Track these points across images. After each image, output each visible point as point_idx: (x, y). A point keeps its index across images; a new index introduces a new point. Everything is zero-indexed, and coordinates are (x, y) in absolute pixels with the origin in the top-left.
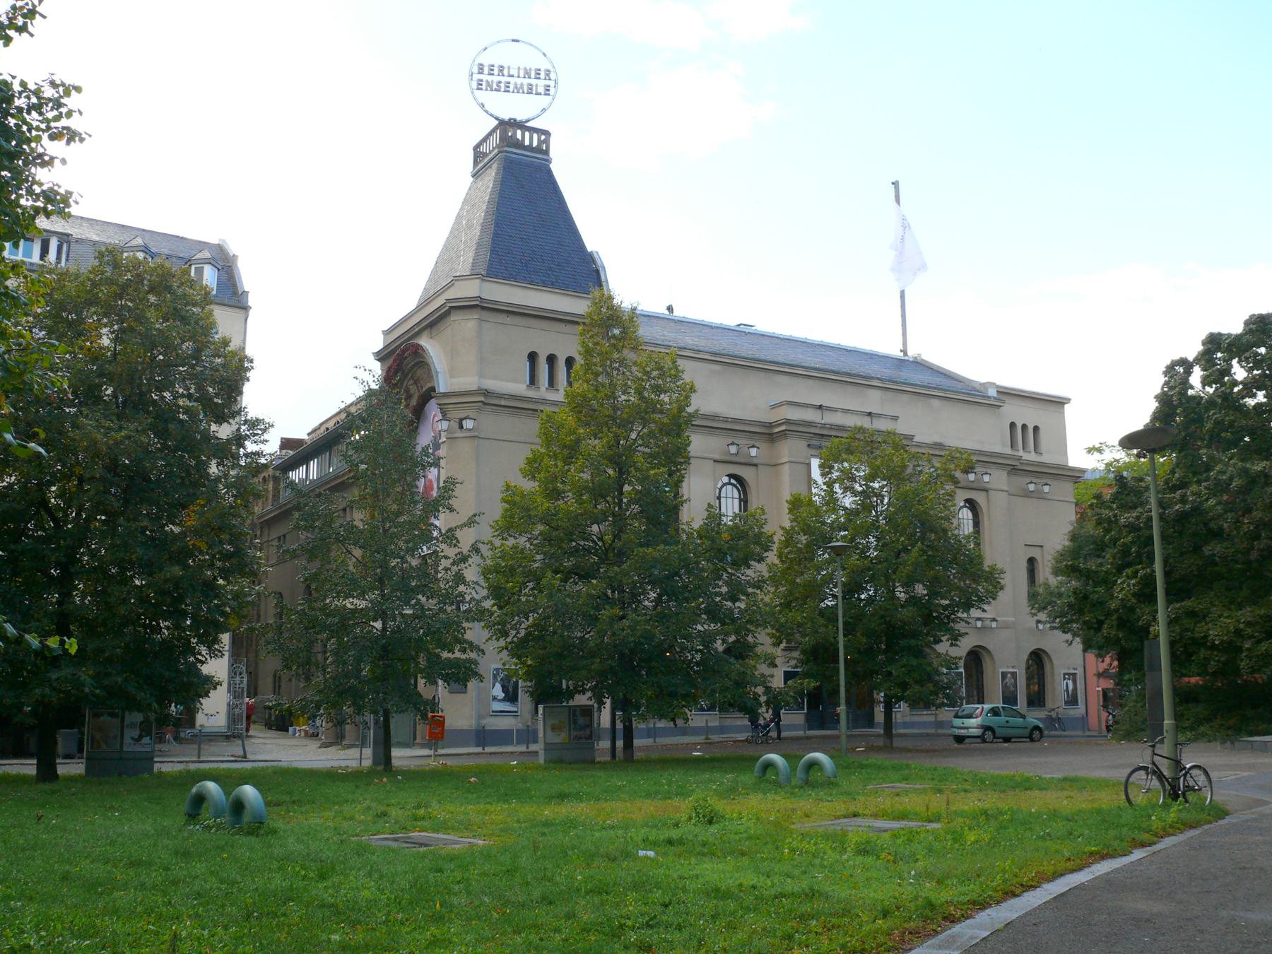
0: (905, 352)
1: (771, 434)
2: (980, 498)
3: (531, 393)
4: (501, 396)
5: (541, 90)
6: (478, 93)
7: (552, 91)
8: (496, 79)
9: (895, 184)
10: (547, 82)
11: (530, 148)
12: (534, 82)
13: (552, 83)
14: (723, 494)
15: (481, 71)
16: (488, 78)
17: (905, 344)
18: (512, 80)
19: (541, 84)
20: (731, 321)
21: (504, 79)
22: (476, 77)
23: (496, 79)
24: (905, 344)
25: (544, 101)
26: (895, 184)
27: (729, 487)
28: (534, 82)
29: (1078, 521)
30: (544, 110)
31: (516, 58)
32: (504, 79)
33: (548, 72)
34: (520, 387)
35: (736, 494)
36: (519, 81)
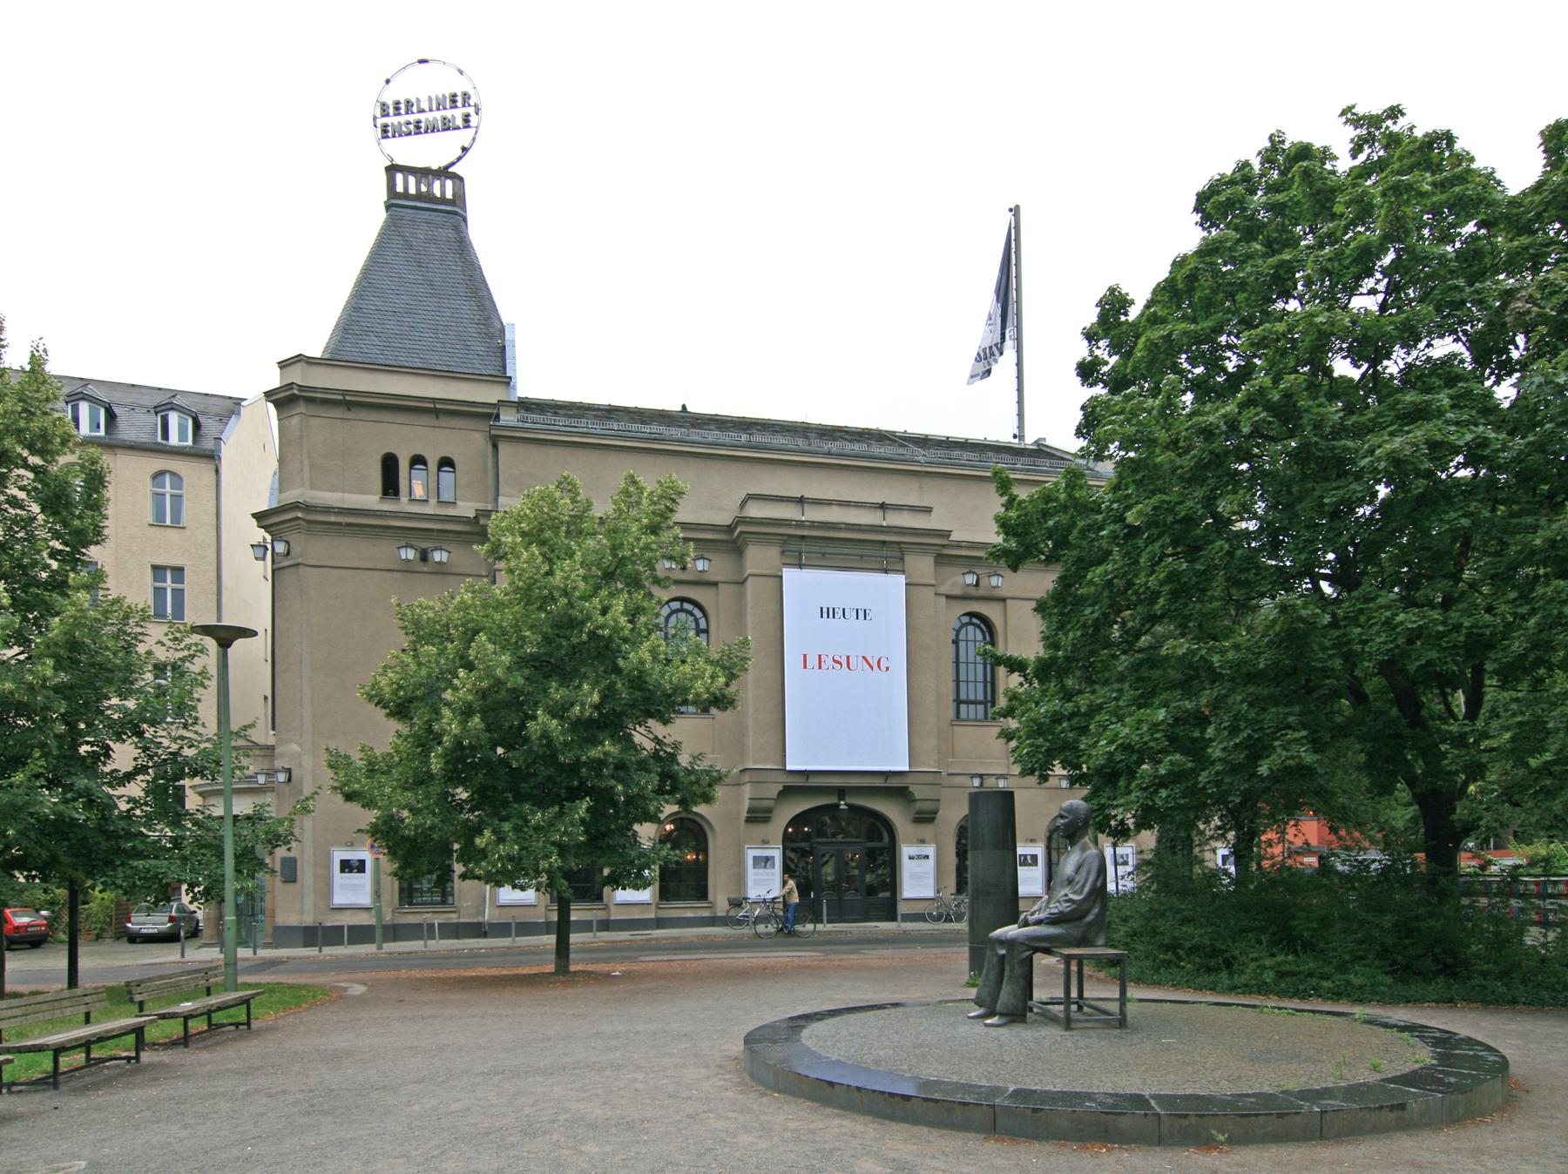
0: (1020, 436)
1: (734, 542)
2: (991, 611)
3: (388, 506)
4: (327, 510)
5: (459, 122)
6: (384, 142)
7: (474, 120)
8: (403, 119)
9: (1016, 211)
10: (466, 110)
11: (443, 200)
12: (448, 113)
13: (471, 110)
14: (962, 636)
15: (385, 114)
16: (396, 119)
17: (1021, 426)
18: (422, 117)
19: (458, 114)
20: (506, 313)
21: (411, 118)
22: (381, 121)
23: (403, 119)
24: (1021, 426)
25: (464, 137)
26: (1016, 211)
27: (971, 628)
28: (448, 113)
29: (1180, 287)
30: (465, 150)
31: (422, 87)
32: (411, 118)
33: (466, 96)
34: (372, 499)
35: (979, 636)
36: (430, 116)
